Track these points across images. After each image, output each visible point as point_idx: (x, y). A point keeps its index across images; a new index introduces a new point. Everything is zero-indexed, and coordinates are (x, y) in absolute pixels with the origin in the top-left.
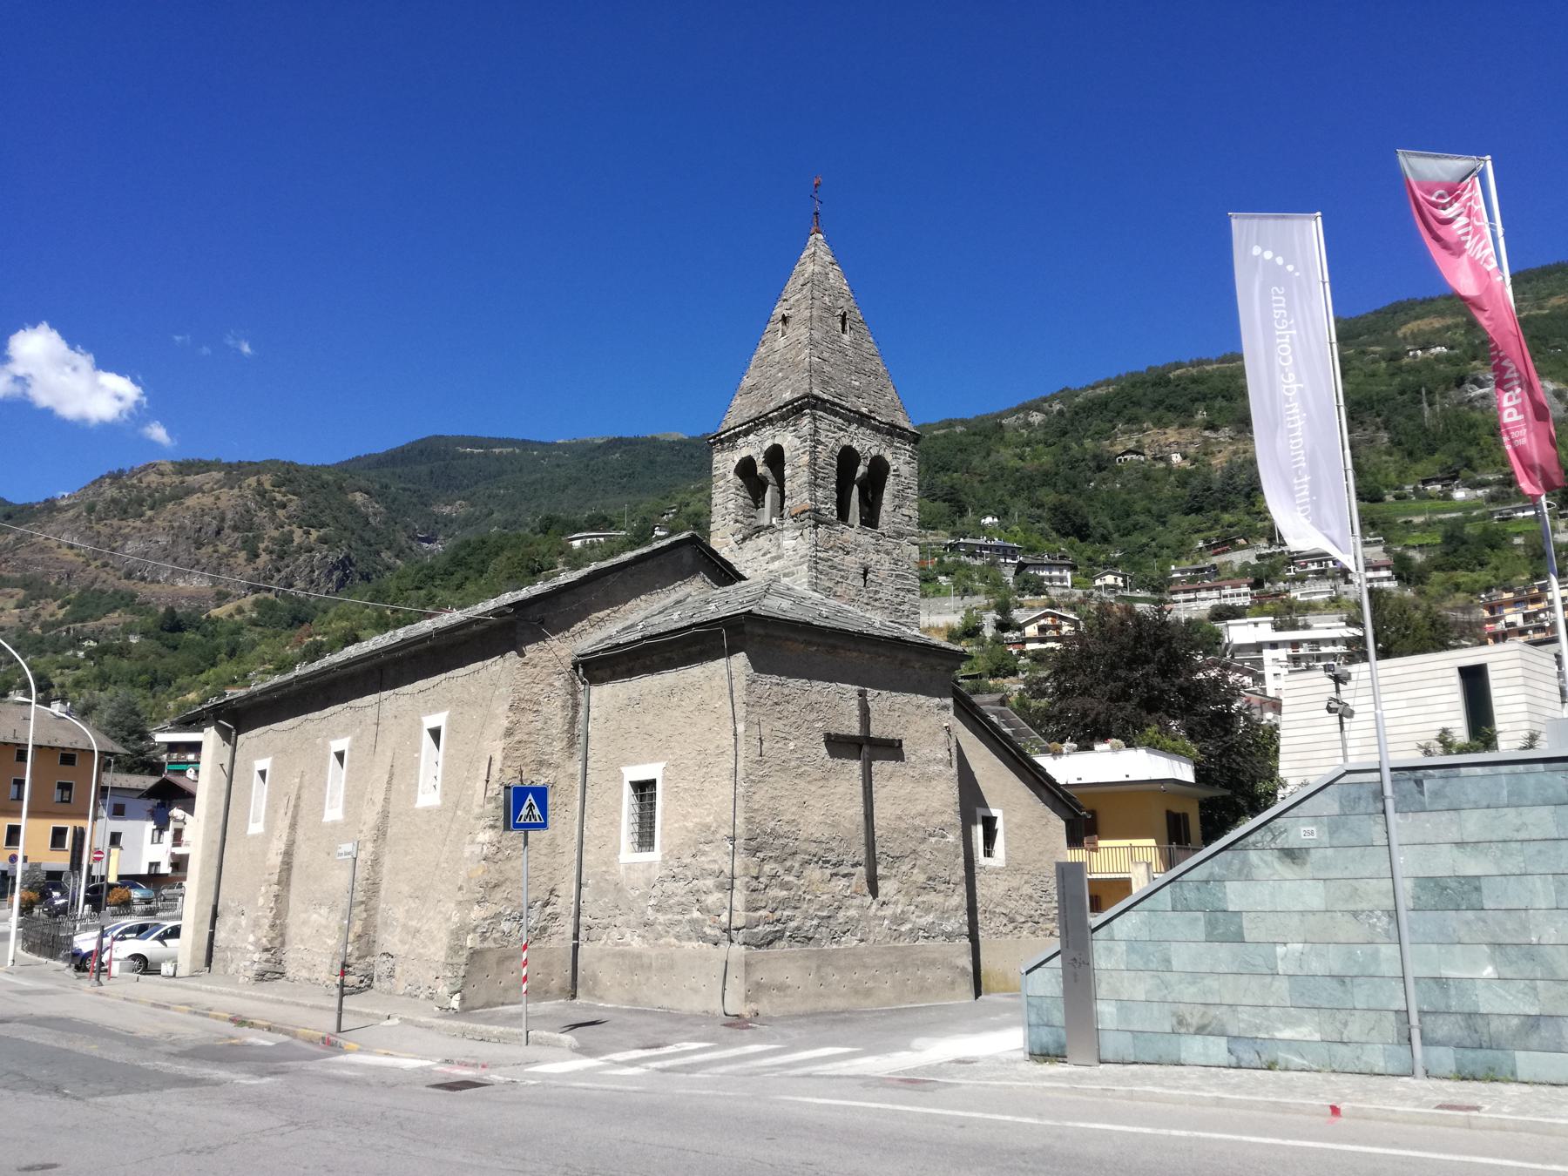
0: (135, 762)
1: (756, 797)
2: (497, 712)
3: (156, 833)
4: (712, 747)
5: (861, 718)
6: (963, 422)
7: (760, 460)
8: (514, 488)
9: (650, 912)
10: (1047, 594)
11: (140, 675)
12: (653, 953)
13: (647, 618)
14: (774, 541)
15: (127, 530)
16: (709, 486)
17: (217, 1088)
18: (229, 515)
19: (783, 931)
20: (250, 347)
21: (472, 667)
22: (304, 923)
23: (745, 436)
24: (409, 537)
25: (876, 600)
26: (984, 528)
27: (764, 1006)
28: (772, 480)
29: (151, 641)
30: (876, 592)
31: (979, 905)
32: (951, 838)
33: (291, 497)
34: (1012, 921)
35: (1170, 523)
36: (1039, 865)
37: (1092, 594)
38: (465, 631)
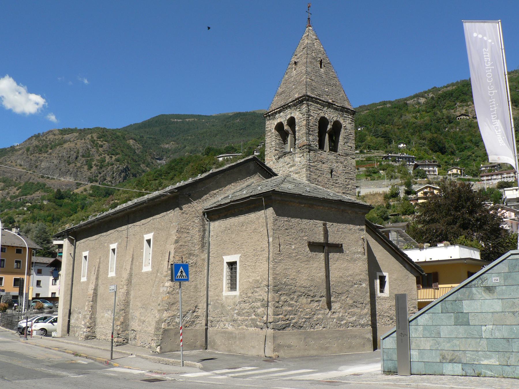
0: (46, 252)
1: (277, 268)
2: (172, 233)
3: (54, 281)
5: (324, 235)
6: (390, 102)
7: (285, 123)
9: (235, 315)
10: (427, 178)
11: (48, 217)
12: (237, 332)
13: (234, 193)
15: (42, 158)
17: (61, 378)
18: (81, 151)
19: (290, 324)
20: (88, 80)
21: (162, 214)
22: (102, 317)
23: (279, 113)
24: (152, 158)
25: (336, 183)
26: (399, 149)
27: (281, 354)
28: (291, 132)
29: (52, 203)
30: (336, 180)
31: (377, 313)
32: (364, 285)
37: (447, 177)
38: (159, 199)
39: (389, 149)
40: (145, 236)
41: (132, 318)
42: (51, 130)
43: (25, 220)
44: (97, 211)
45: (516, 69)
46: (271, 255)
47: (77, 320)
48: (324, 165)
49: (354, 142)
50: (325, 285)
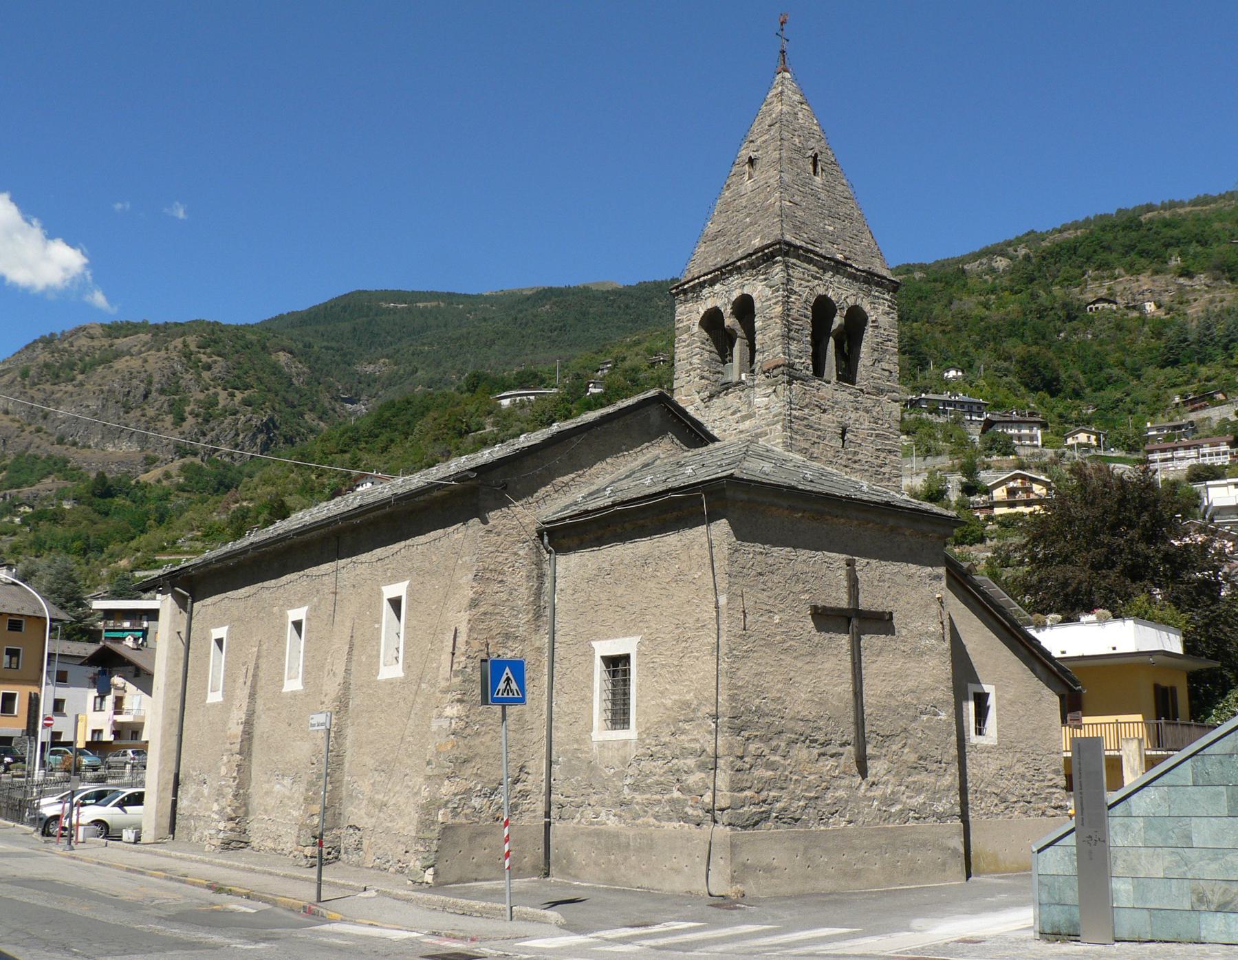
1: (740, 673)
2: (461, 582)
3: (98, 700)
4: (691, 621)
5: (849, 590)
6: (922, 267)
7: (727, 311)
8: (438, 344)
9: (626, 790)
10: (1015, 453)
11: (73, 541)
12: (631, 834)
13: (613, 482)
14: (744, 399)
15: (58, 395)
16: (671, 343)
18: (156, 379)
19: (769, 812)
21: (433, 534)
25: (855, 462)
26: (947, 382)
27: (751, 888)
28: (740, 332)
29: (83, 507)
30: (855, 453)
31: (969, 785)
32: (943, 716)
33: (216, 358)
34: (1004, 801)
35: (1145, 376)
36: (1032, 743)
37: (1064, 454)
39: (920, 381)
40: (384, 589)
41: (351, 795)
42: (83, 324)
43: (16, 548)
44: (198, 527)
45: (1230, 190)
46: (723, 639)
47: (196, 799)
48: (825, 416)
49: (895, 359)
50: (852, 714)
